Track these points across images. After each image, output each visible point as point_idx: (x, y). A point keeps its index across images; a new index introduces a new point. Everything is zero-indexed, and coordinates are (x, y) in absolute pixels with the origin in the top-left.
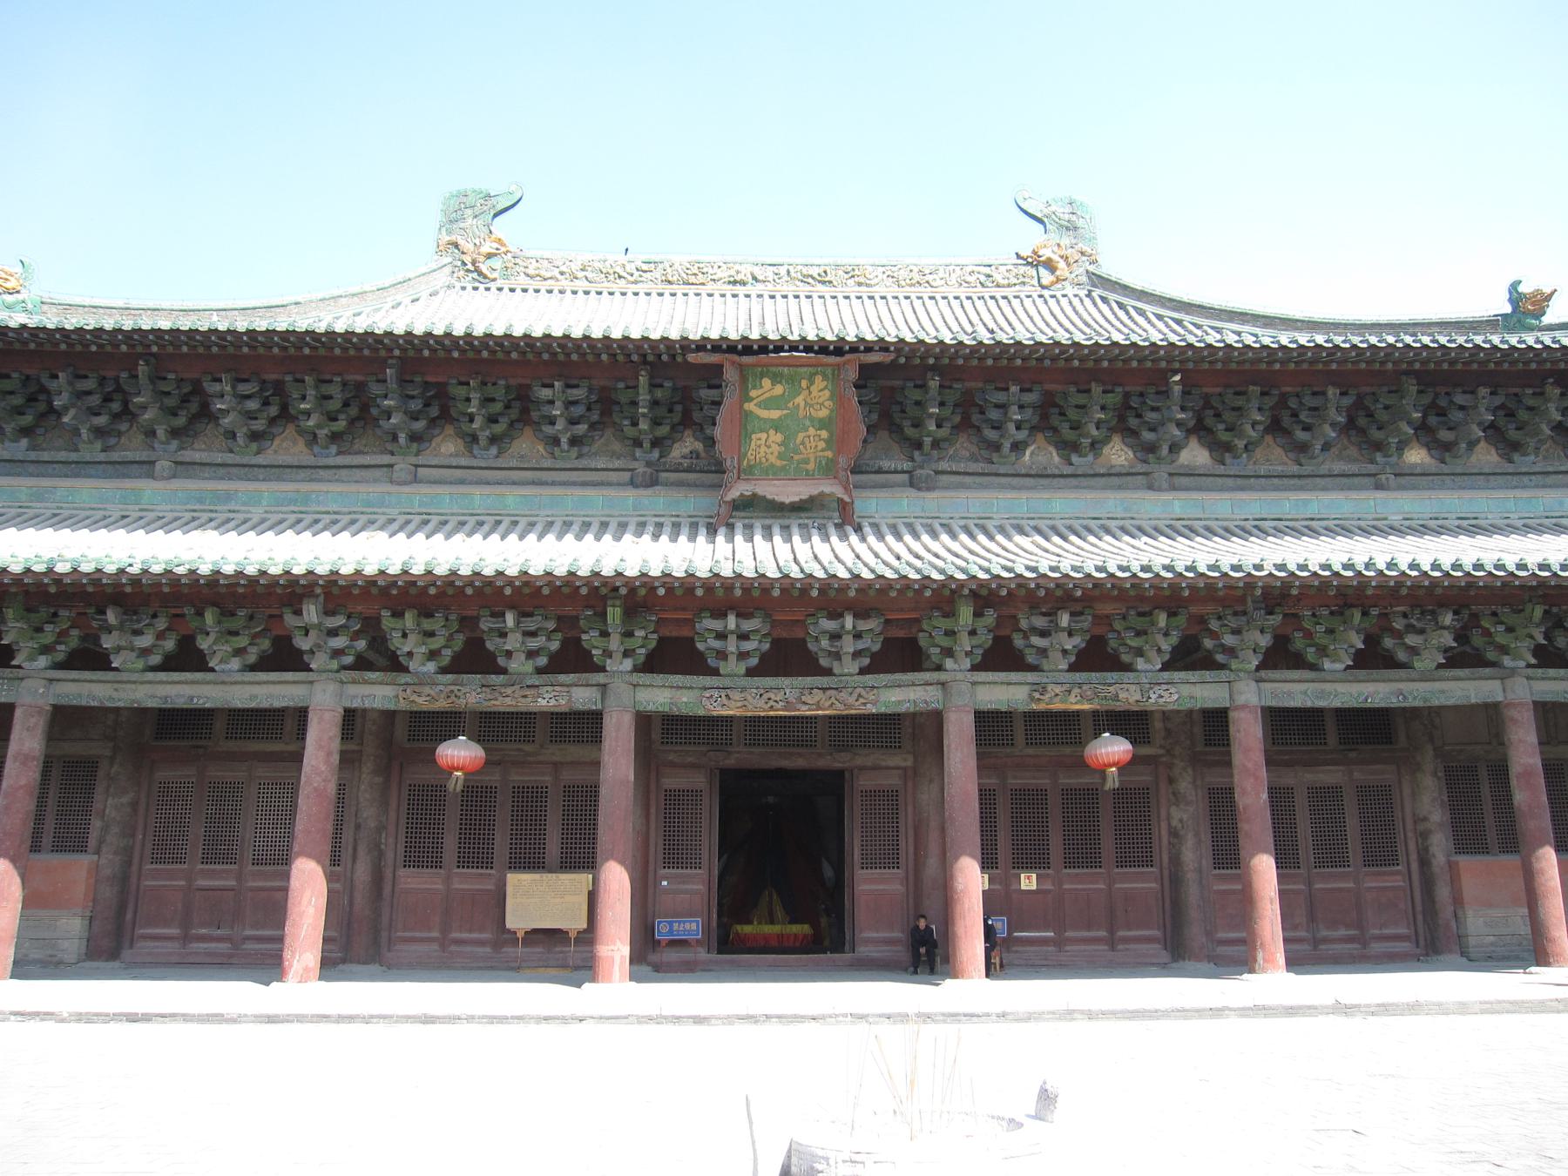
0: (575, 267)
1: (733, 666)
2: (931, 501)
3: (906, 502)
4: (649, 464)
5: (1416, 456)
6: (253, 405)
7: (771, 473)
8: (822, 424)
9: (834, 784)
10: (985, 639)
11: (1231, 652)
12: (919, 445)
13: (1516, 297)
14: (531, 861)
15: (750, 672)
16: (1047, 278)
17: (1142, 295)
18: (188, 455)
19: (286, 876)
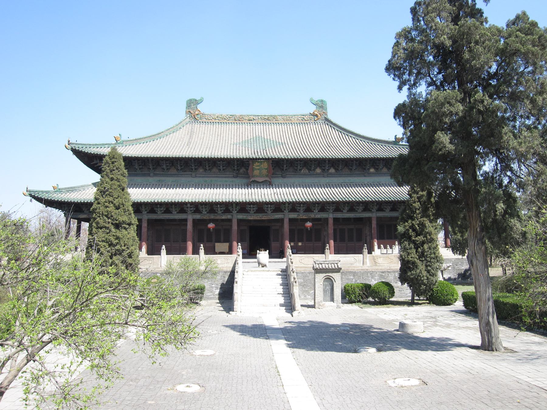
1: (252, 212)
2: (285, 180)
3: (281, 180)
5: (372, 170)
7: (257, 176)
8: (266, 169)
9: (269, 227)
11: (329, 209)
12: (283, 170)
14: (219, 241)
16: (316, 119)
17: (335, 125)
19: (186, 244)
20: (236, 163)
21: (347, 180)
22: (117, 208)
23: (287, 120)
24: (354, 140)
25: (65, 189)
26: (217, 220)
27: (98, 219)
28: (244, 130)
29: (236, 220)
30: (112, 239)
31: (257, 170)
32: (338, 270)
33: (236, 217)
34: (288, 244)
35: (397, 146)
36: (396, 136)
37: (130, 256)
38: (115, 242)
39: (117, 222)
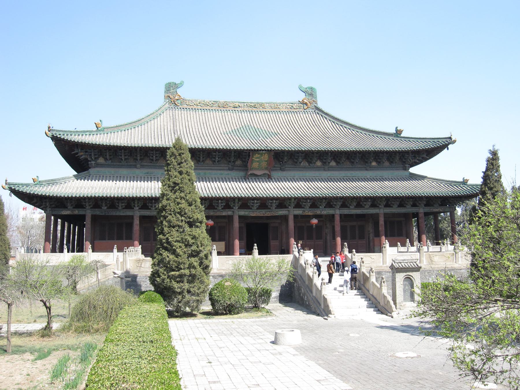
0: (198, 103)
2: (284, 173)
3: (280, 174)
4: (232, 166)
5: (374, 164)
7: (256, 169)
8: (266, 161)
10: (295, 203)
11: (335, 205)
13: (397, 130)
16: (306, 107)
18: (143, 164)
20: (233, 154)
21: (349, 173)
22: (190, 205)
23: (275, 108)
24: (349, 131)
25: (45, 181)
26: (218, 217)
27: (170, 217)
28: (230, 118)
29: (292, 217)
30: (189, 238)
31: (256, 162)
32: (417, 269)
33: (238, 213)
34: (292, 241)
35: (398, 139)
36: (397, 128)
37: (206, 256)
38: (191, 241)
39: (191, 220)
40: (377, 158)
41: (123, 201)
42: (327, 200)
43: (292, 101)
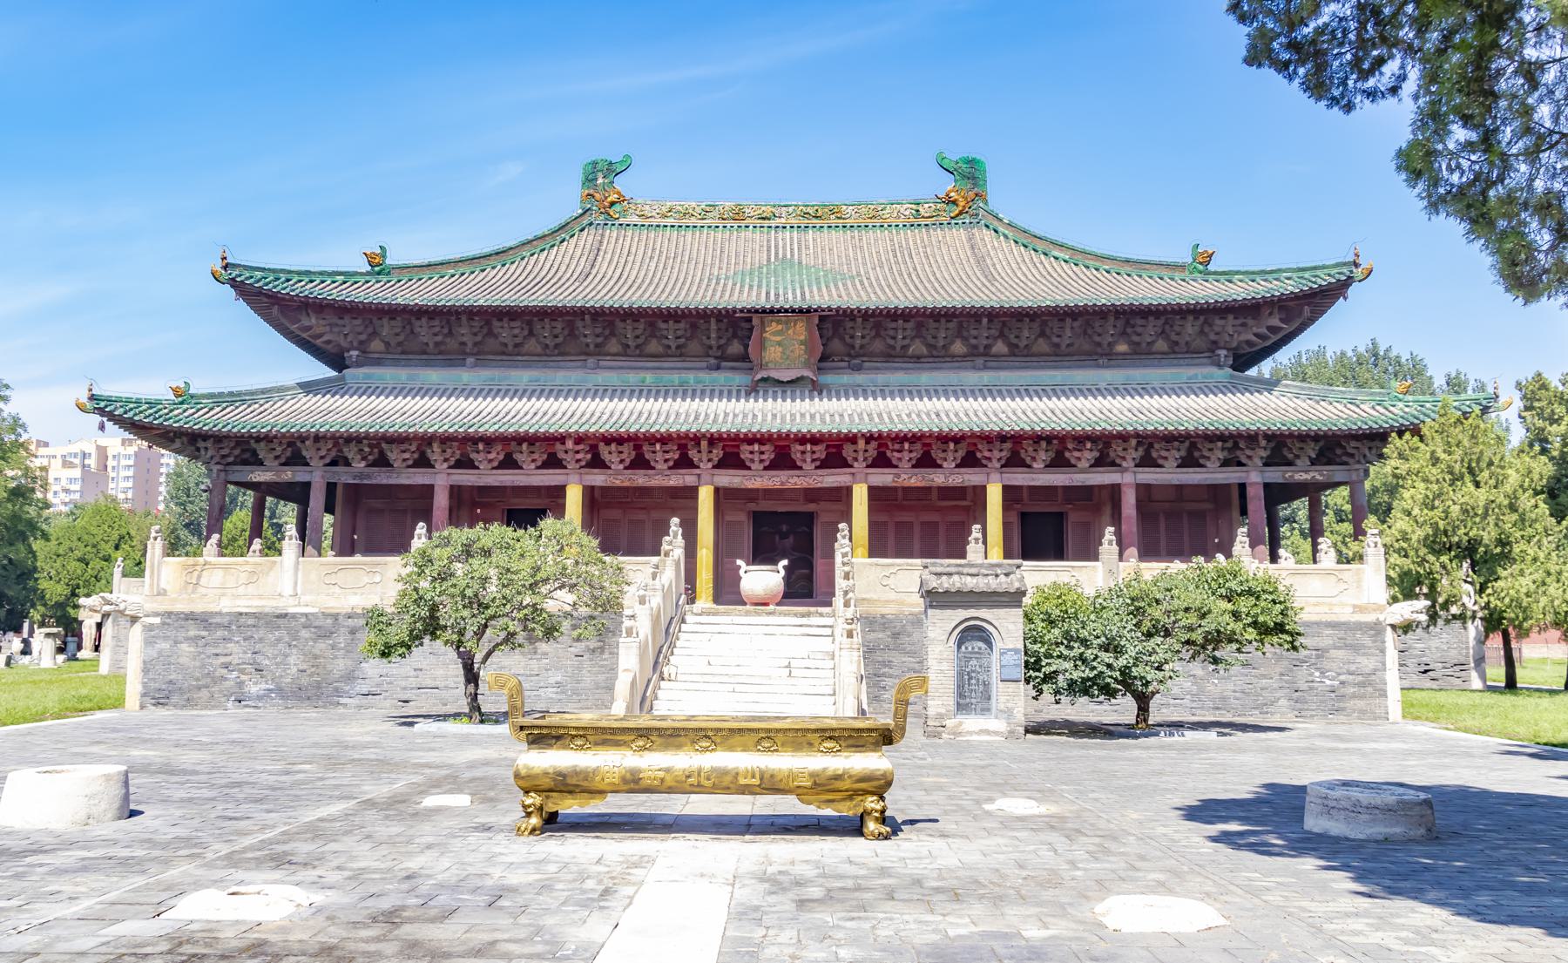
2: (860, 378)
3: (846, 378)
6: (516, 331)
8: (802, 343)
11: (989, 459)
15: (766, 468)
40: (1129, 330)
41: (405, 446)
42: (964, 445)
43: (918, 196)
